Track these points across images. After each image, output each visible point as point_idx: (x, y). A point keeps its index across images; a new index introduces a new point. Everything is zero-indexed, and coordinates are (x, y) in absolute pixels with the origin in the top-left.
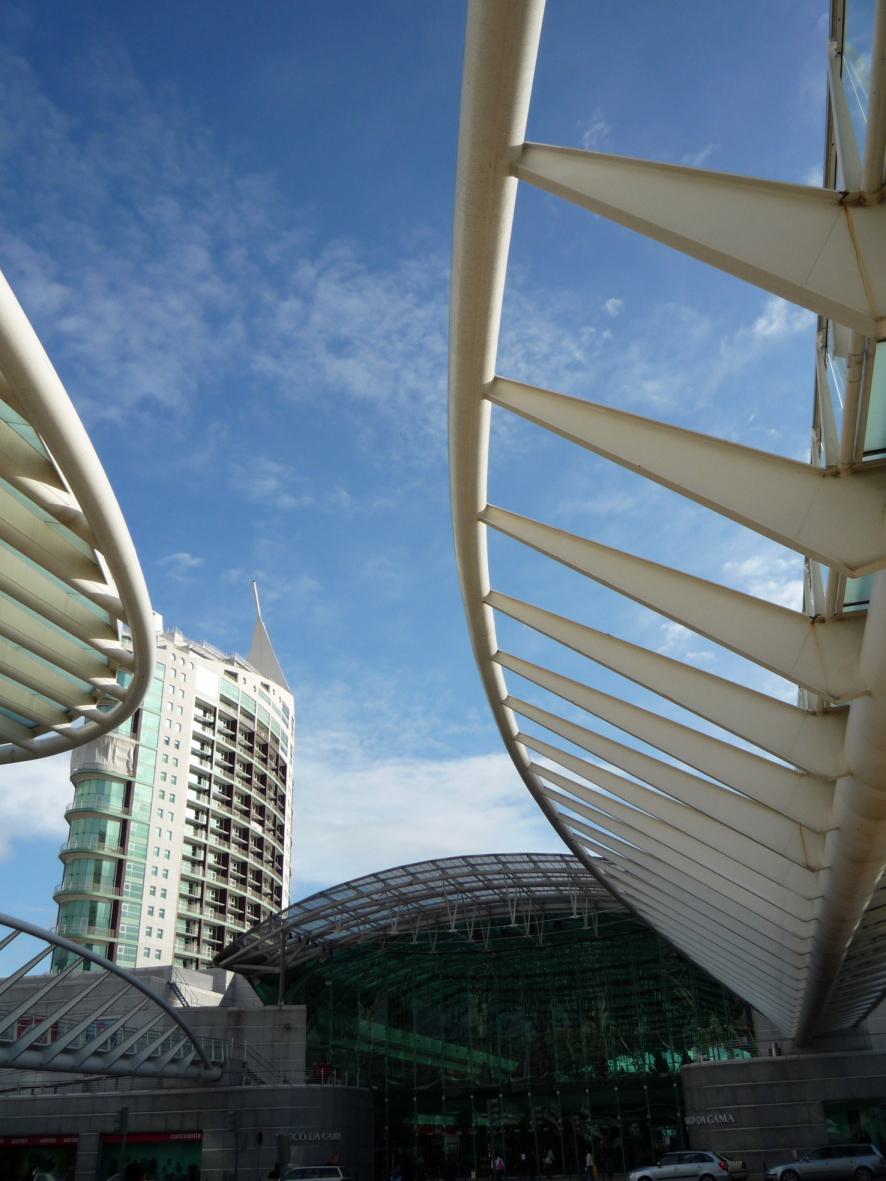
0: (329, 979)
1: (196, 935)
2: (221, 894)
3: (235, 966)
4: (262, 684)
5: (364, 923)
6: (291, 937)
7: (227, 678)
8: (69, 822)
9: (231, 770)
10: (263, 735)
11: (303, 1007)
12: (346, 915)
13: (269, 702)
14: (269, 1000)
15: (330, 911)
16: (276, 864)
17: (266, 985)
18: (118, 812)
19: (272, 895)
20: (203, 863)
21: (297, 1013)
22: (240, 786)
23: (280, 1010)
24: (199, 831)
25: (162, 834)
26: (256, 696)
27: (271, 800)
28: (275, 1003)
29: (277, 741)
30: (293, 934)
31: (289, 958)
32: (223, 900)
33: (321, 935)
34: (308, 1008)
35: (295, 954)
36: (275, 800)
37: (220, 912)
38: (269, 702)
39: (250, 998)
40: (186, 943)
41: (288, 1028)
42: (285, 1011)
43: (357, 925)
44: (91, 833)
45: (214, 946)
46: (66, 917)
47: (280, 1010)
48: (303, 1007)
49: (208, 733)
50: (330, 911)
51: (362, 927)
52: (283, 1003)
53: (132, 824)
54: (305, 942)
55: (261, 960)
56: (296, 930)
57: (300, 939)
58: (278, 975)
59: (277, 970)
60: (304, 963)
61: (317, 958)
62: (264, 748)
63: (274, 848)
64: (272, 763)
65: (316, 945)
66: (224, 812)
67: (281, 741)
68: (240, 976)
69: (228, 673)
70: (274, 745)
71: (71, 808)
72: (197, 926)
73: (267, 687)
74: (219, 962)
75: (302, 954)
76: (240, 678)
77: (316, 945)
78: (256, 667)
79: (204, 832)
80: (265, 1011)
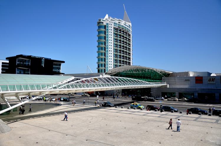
76: (121, 23)
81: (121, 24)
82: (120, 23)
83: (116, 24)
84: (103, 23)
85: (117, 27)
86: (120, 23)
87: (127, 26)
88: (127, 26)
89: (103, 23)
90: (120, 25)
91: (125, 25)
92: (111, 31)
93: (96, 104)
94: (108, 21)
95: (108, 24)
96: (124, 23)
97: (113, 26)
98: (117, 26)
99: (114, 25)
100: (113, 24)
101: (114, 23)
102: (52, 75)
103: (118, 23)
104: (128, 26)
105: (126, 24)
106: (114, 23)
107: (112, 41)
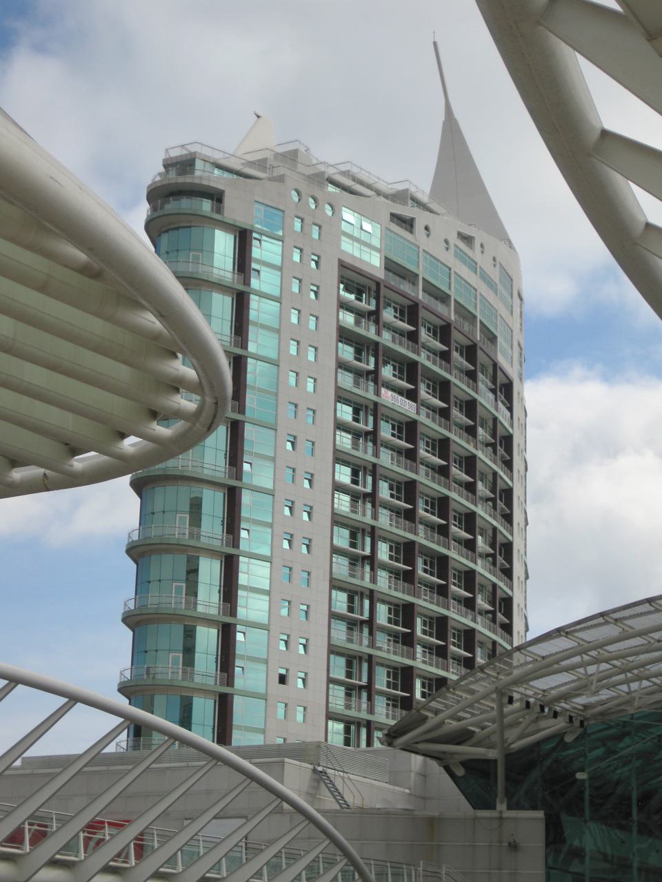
0: (582, 770)
1: (366, 616)
2: (405, 613)
3: (421, 746)
5: (639, 678)
6: (511, 701)
7: (395, 228)
8: (140, 494)
9: (411, 455)
10: (466, 327)
11: (540, 814)
12: (604, 666)
13: (473, 265)
14: (481, 801)
15: (577, 659)
16: (500, 559)
17: (477, 780)
18: (211, 681)
19: (493, 500)
20: (371, 559)
21: (529, 824)
22: (428, 422)
23: (501, 818)
24: (362, 380)
25: (294, 576)
26: (449, 258)
27: (487, 445)
28: (492, 807)
29: (493, 339)
30: (516, 696)
31: (511, 734)
32: (409, 623)
33: (565, 697)
34: (545, 814)
35: (522, 726)
36: (493, 446)
37: (404, 643)
38: (473, 265)
39: (449, 796)
40: (350, 629)
41: (514, 847)
42: (509, 818)
43: (627, 682)
44: (170, 651)
45: (394, 701)
46: (168, 253)
47: (501, 818)
48: (540, 814)
49: (367, 392)
50: (577, 659)
51: (634, 686)
52: (504, 806)
53: (248, 427)
54: (538, 709)
55: (463, 737)
56: (521, 690)
57: (528, 704)
58: (495, 761)
59: (492, 754)
60: (538, 744)
61: (559, 736)
62: (470, 352)
63: (495, 474)
64: (483, 382)
65: (555, 715)
66: (404, 472)
67: (500, 339)
68: (433, 764)
69: (397, 218)
70: (487, 346)
71: (135, 537)
72: (365, 666)
73: (467, 239)
74: (395, 738)
75: (531, 729)
76: (419, 227)
77: (555, 715)
78: (414, 576)
79: (369, 506)
80: (475, 819)
84: (217, 197)
87: (484, 277)
96: (454, 240)
105: (476, 255)
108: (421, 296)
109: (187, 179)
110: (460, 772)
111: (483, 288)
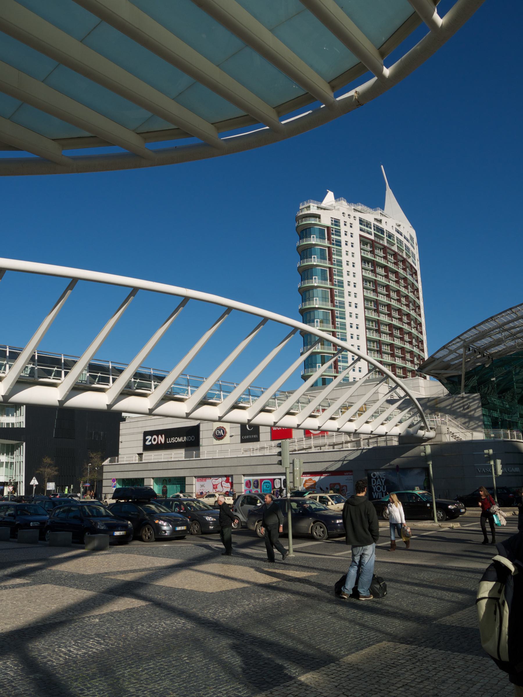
4: (375, 219)
81: (383, 226)
82: (380, 221)
83: (368, 225)
85: (372, 237)
86: (380, 221)
88: (405, 238)
89: (318, 217)
90: (382, 231)
91: (398, 232)
92: (354, 331)
93: (441, 433)
94: (338, 209)
95: (336, 222)
96: (395, 226)
97: (357, 232)
98: (370, 233)
99: (361, 230)
100: (357, 225)
101: (361, 221)
102: (188, 353)
103: (373, 222)
104: (409, 238)
106: (361, 221)
107: (361, 310)
108: (386, 245)
109: (309, 212)
110: (445, 381)
111: (405, 241)
